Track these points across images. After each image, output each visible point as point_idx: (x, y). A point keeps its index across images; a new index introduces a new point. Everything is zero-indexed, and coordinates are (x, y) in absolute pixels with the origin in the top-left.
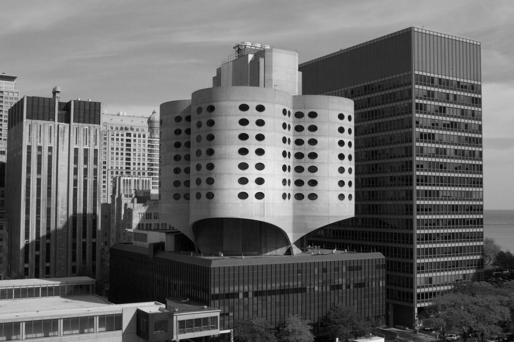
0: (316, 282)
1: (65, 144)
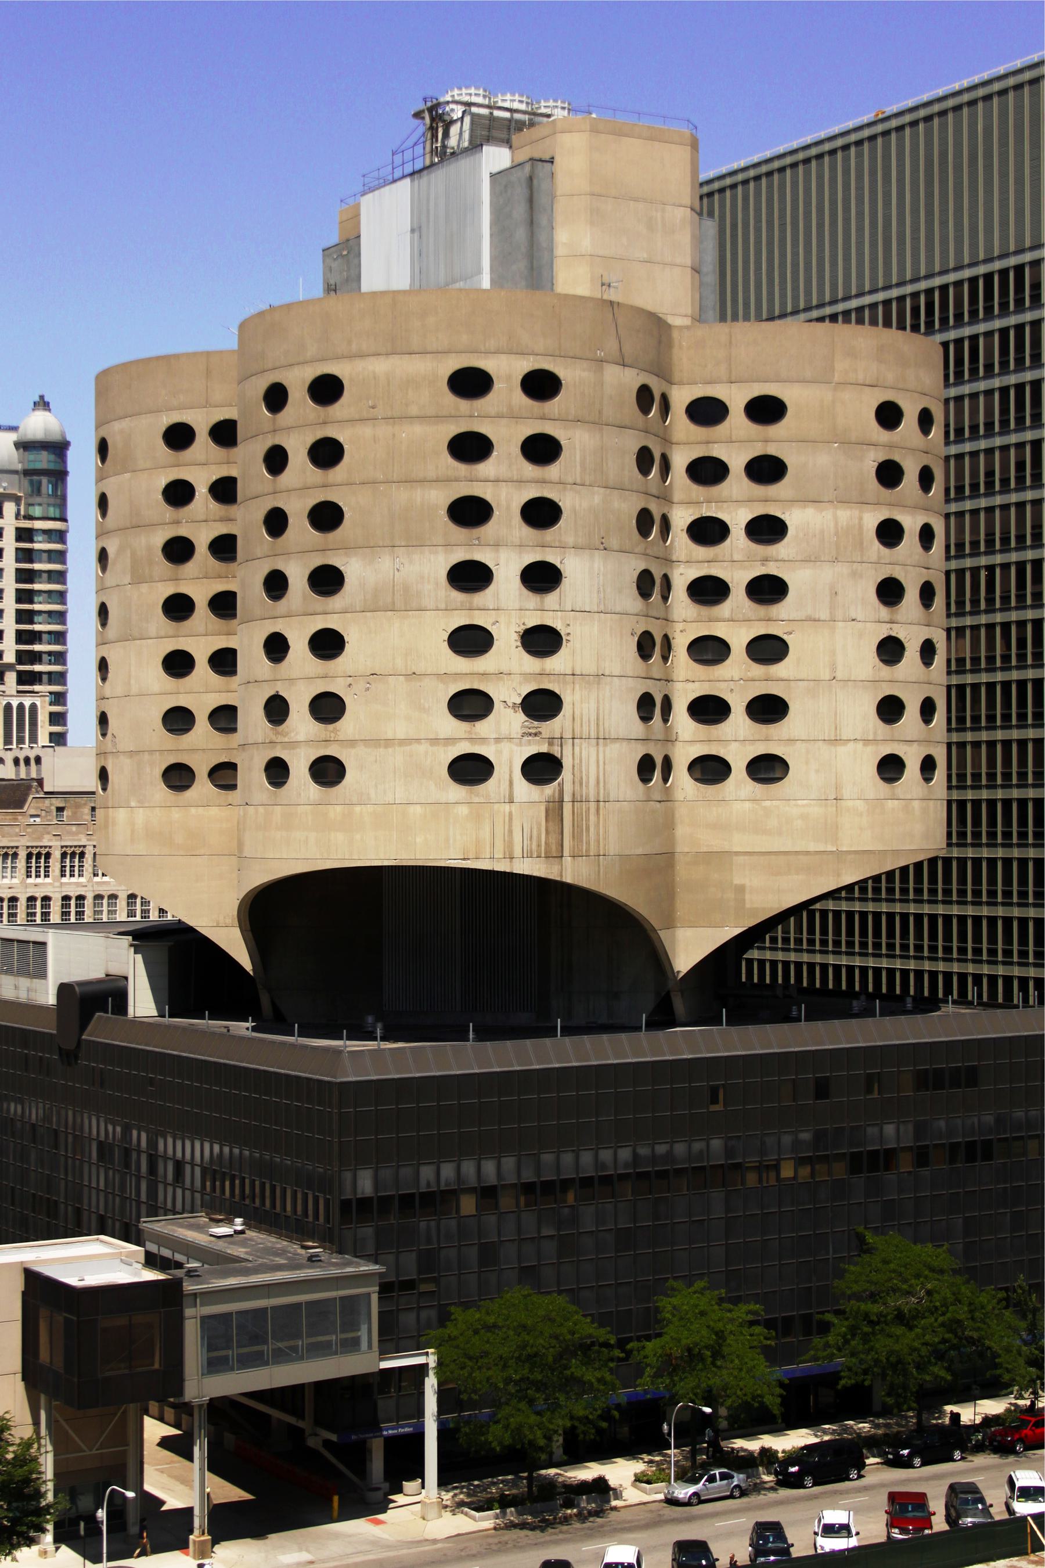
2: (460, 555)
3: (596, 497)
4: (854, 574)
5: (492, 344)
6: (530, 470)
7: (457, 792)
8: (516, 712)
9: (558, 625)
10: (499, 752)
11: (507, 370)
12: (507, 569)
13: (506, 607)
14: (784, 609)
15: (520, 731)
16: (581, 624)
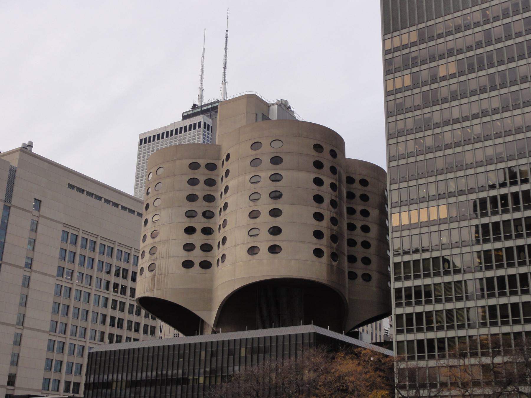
0: (202, 371)
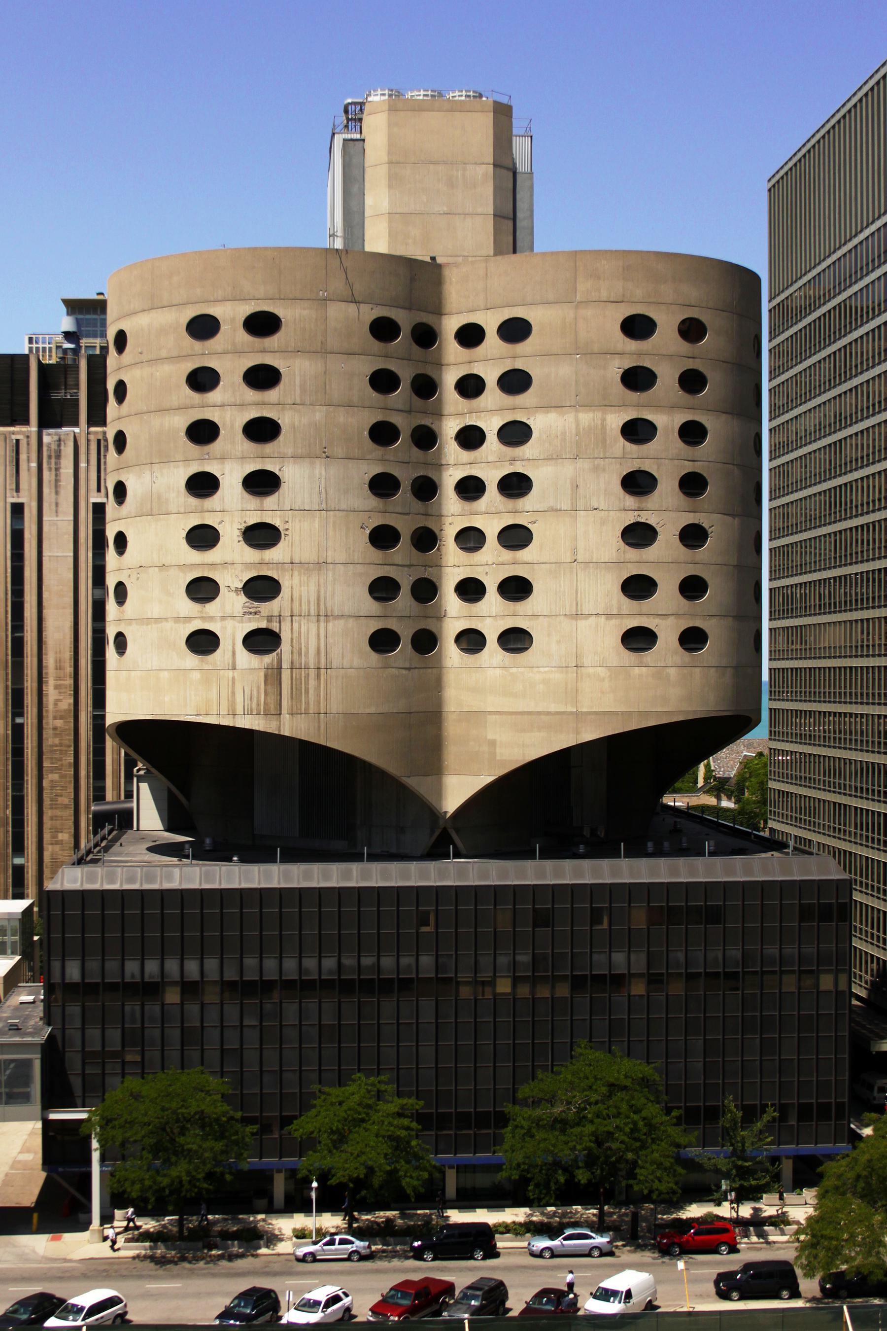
1: (62, 492)
2: (195, 468)
3: (317, 414)
4: (596, 469)
5: (220, 294)
6: (251, 395)
7: (192, 660)
8: (238, 595)
9: (277, 522)
10: (224, 628)
11: (231, 315)
12: (231, 479)
13: (231, 509)
14: (528, 502)
15: (242, 611)
16: (300, 521)
